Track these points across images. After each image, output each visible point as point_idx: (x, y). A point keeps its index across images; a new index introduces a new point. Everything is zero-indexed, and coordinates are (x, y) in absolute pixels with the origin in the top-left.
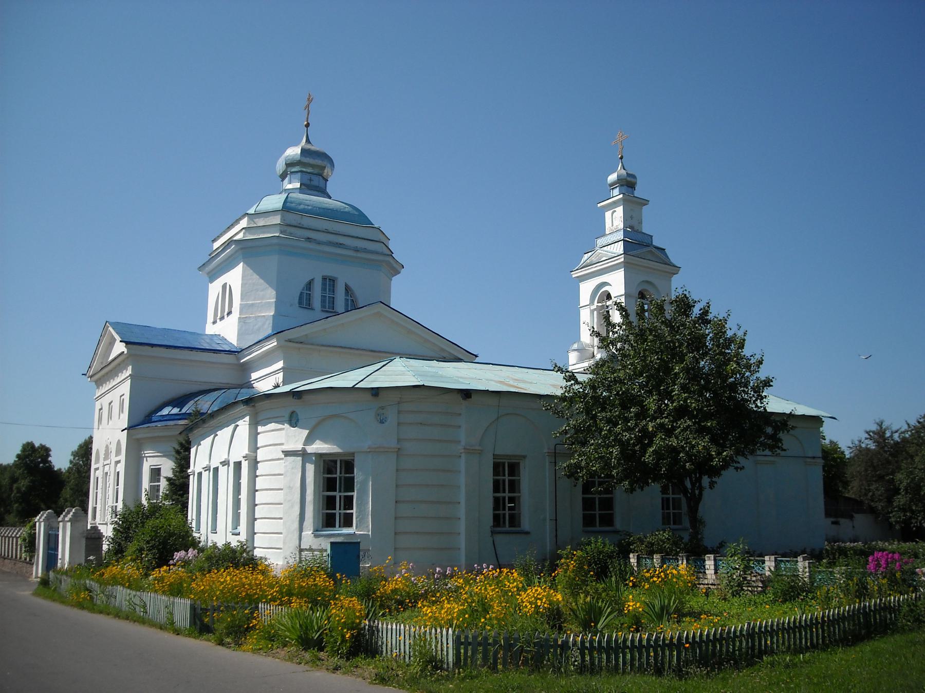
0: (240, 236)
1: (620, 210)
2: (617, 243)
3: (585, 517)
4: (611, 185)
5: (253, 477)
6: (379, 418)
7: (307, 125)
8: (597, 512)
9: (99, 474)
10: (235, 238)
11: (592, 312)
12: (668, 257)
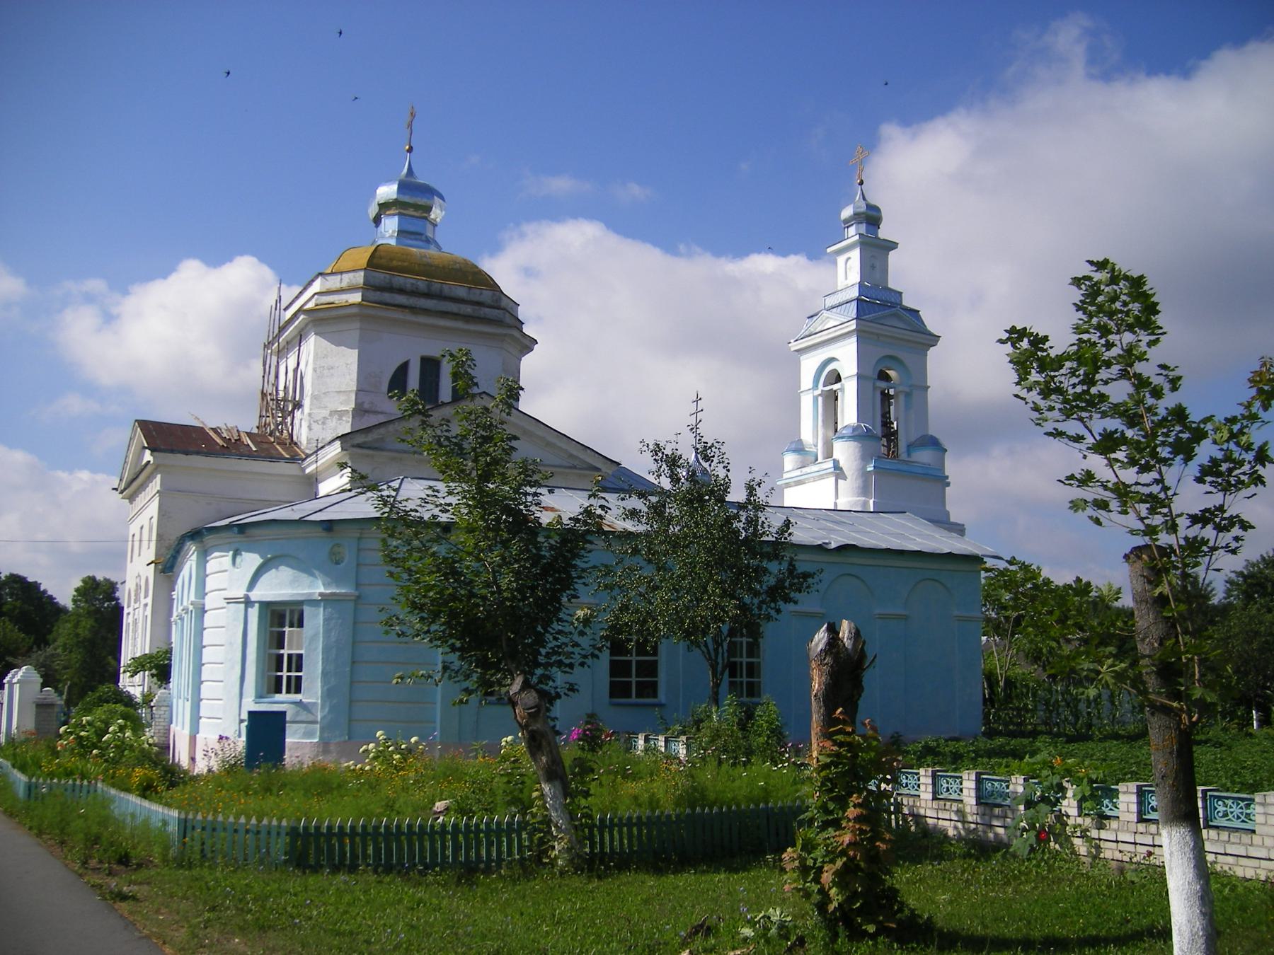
0: (311, 305)
1: (855, 255)
2: (848, 304)
3: (612, 684)
4: (846, 221)
5: (200, 630)
6: (334, 557)
7: (410, 150)
8: (634, 679)
9: (131, 619)
10: (306, 307)
11: (815, 399)
12: (923, 323)
